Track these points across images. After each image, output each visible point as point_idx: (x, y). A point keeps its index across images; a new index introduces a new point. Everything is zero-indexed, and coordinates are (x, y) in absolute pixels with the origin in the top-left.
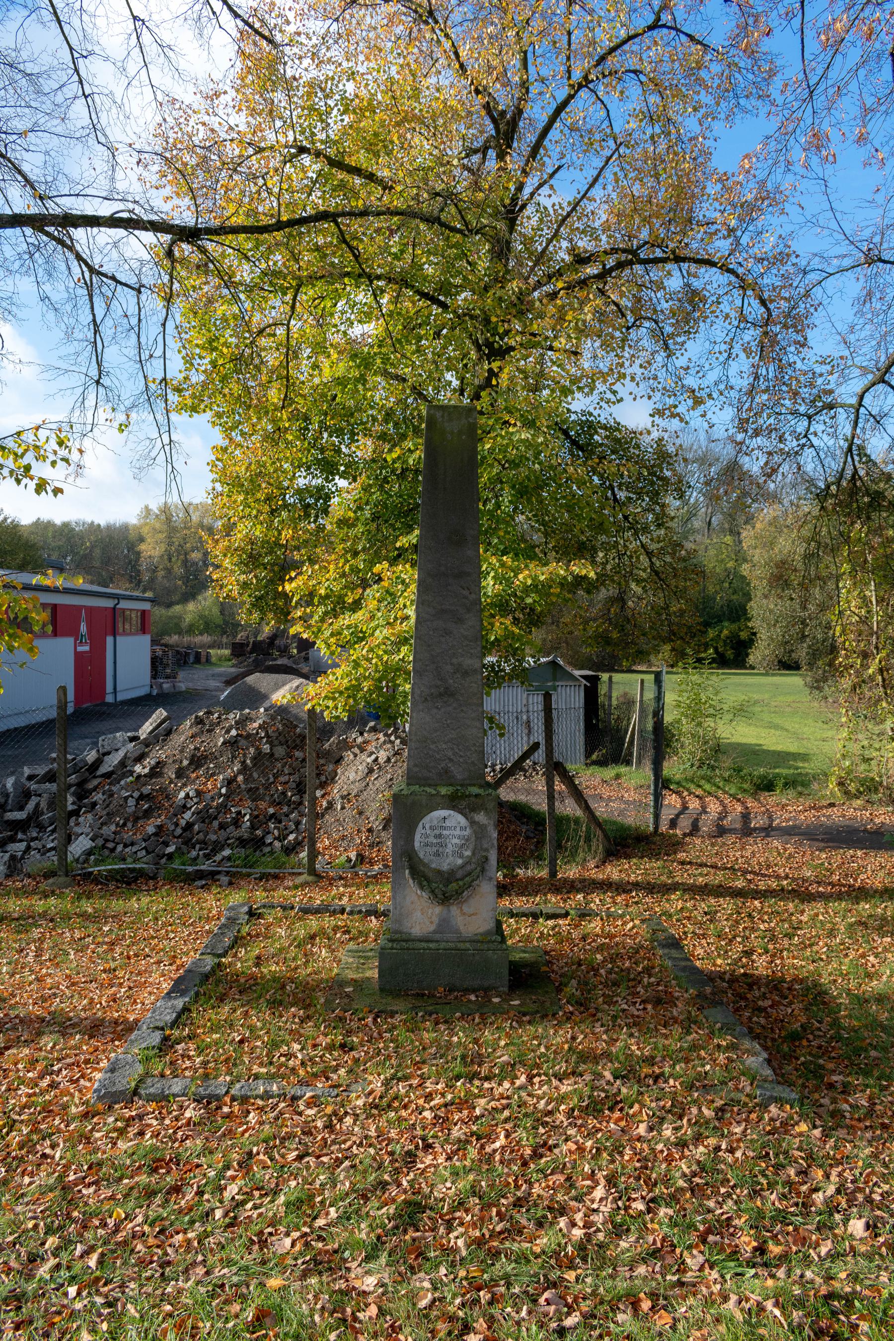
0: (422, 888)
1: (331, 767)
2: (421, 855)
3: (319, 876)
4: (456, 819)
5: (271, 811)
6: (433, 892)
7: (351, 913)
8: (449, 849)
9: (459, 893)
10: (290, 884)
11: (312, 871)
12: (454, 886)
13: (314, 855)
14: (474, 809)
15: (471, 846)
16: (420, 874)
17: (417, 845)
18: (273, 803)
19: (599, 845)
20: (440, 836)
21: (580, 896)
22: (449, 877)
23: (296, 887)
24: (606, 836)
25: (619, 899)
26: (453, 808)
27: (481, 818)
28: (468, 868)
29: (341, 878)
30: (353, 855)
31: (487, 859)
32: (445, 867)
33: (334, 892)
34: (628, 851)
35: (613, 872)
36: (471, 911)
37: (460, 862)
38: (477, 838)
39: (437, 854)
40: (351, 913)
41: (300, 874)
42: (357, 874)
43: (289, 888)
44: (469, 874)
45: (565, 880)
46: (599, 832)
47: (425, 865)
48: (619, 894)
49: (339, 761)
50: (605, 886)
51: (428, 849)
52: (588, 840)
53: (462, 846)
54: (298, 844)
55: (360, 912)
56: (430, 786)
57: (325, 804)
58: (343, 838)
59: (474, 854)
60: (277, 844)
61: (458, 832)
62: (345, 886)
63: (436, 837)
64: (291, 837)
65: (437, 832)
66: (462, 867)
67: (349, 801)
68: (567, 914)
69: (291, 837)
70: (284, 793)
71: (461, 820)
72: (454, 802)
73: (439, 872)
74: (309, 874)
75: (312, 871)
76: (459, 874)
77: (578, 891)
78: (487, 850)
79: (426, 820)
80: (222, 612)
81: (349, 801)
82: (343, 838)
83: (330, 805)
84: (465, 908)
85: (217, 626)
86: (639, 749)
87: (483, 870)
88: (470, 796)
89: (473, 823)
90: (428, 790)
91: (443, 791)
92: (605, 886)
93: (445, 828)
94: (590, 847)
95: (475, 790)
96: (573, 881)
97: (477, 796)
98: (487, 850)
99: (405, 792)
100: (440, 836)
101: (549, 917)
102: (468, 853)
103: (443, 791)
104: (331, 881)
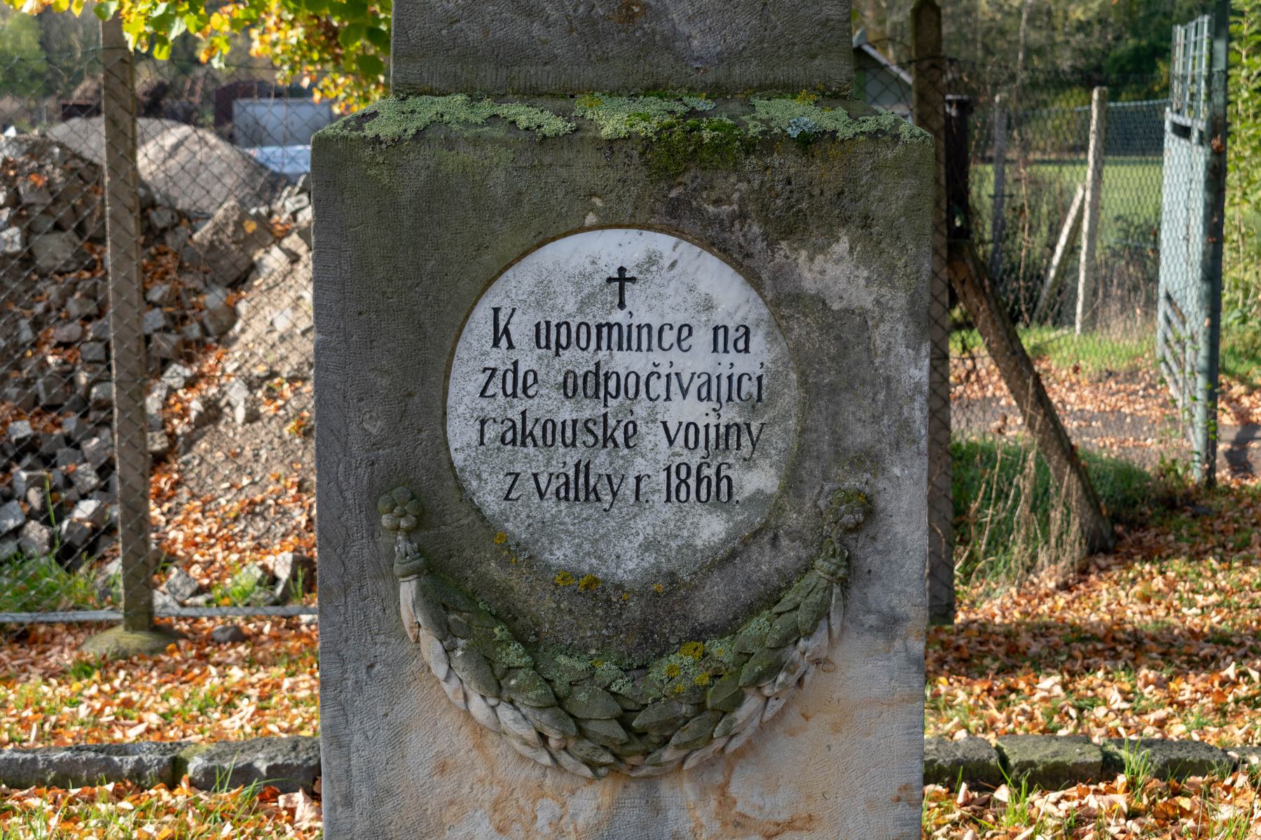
0: (496, 684)
1: (214, 298)
2: (489, 497)
3: (164, 633)
4: (689, 283)
5: (22, 429)
6: (558, 703)
7: (207, 781)
8: (652, 457)
9: (709, 709)
10: (68, 659)
11: (142, 616)
12: (680, 667)
13: (149, 565)
14: (791, 224)
15: (779, 440)
16: (487, 606)
17: (461, 434)
18: (31, 407)
19: (1069, 522)
20: (595, 383)
21: (1050, 683)
22: (650, 618)
23: (84, 670)
24: (1090, 494)
25: (1185, 689)
26: (674, 218)
27: (834, 271)
28: (765, 563)
29: (238, 637)
30: (281, 564)
31: (869, 509)
32: (628, 562)
33: (213, 680)
34: (1148, 537)
35: (1117, 599)
36: (780, 805)
37: (712, 528)
38: (811, 391)
39: (580, 488)
40: (207, 781)
41: (111, 625)
42: (293, 626)
43: (61, 674)
44: (771, 598)
45: (984, 631)
46: (1070, 480)
47: (516, 553)
48: (1180, 674)
49: (241, 278)
50: (1120, 646)
51: (529, 460)
52: (1040, 503)
53: (726, 437)
54: (101, 531)
55: (244, 775)
56: (531, 94)
57: (196, 406)
58: (252, 510)
59: (792, 482)
60: (37, 532)
61: (699, 359)
62: (250, 663)
63: (570, 387)
64: (86, 509)
65: (578, 360)
66: (727, 557)
67: (272, 395)
68: (1109, 767)
69: (86, 509)
70: (67, 376)
71: (724, 290)
72: (674, 182)
73: (594, 591)
74: (133, 624)
75: (142, 616)
76: (711, 601)
77: (1040, 665)
78: (869, 460)
79: (515, 289)
80: (44, 44)
81: (272, 395)
82: (252, 510)
83: (213, 413)
84: (746, 791)
85: (35, 75)
86: (1092, 293)
87: (848, 576)
88: (768, 143)
89: (786, 303)
90: (523, 114)
91: (612, 120)
92: (1120, 646)
93: (625, 338)
94: (1045, 522)
95: (796, 114)
96: (1010, 634)
97: (808, 142)
98: (869, 460)
99: (384, 128)
100: (595, 383)
101: (1053, 777)
102: (759, 480)
103: (612, 120)
104: (206, 647)
